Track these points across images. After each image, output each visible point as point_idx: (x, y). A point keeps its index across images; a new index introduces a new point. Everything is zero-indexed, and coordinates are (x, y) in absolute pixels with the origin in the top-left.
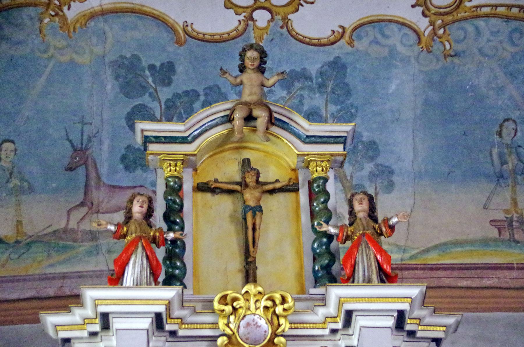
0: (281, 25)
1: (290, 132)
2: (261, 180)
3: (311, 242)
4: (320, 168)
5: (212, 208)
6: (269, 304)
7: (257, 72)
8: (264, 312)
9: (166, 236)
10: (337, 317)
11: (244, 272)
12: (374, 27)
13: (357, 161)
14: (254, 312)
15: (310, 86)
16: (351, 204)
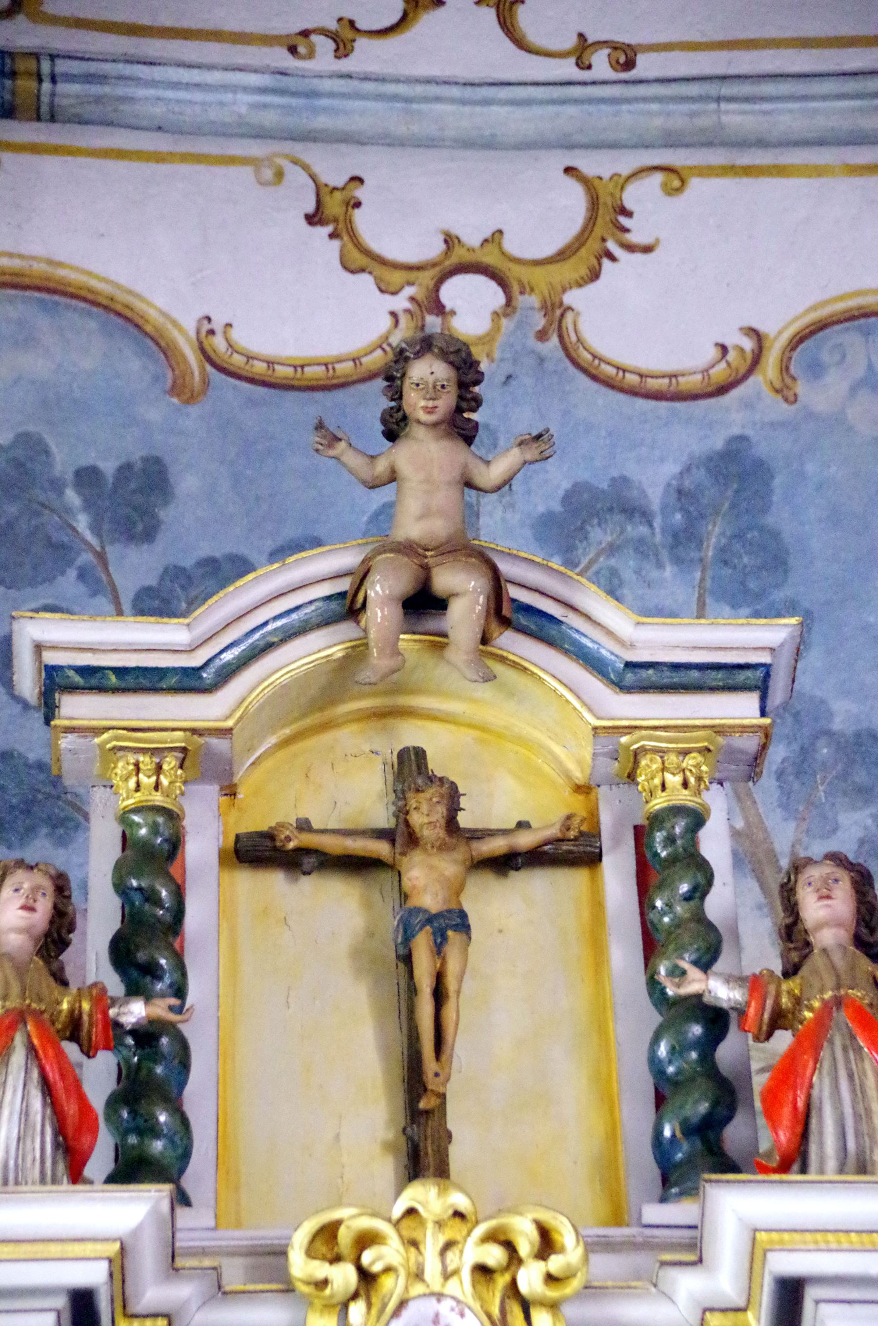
0: (540, 327)
1: (566, 652)
2: (464, 820)
3: (649, 1035)
4: (674, 774)
5: (290, 923)
6: (494, 1255)
7: (448, 435)
8: (474, 1287)
9: (118, 1014)
10: (744, 1310)
11: (405, 1154)
12: (867, 333)
13: (810, 803)
14: (436, 1287)
15: (641, 541)
16: (789, 901)
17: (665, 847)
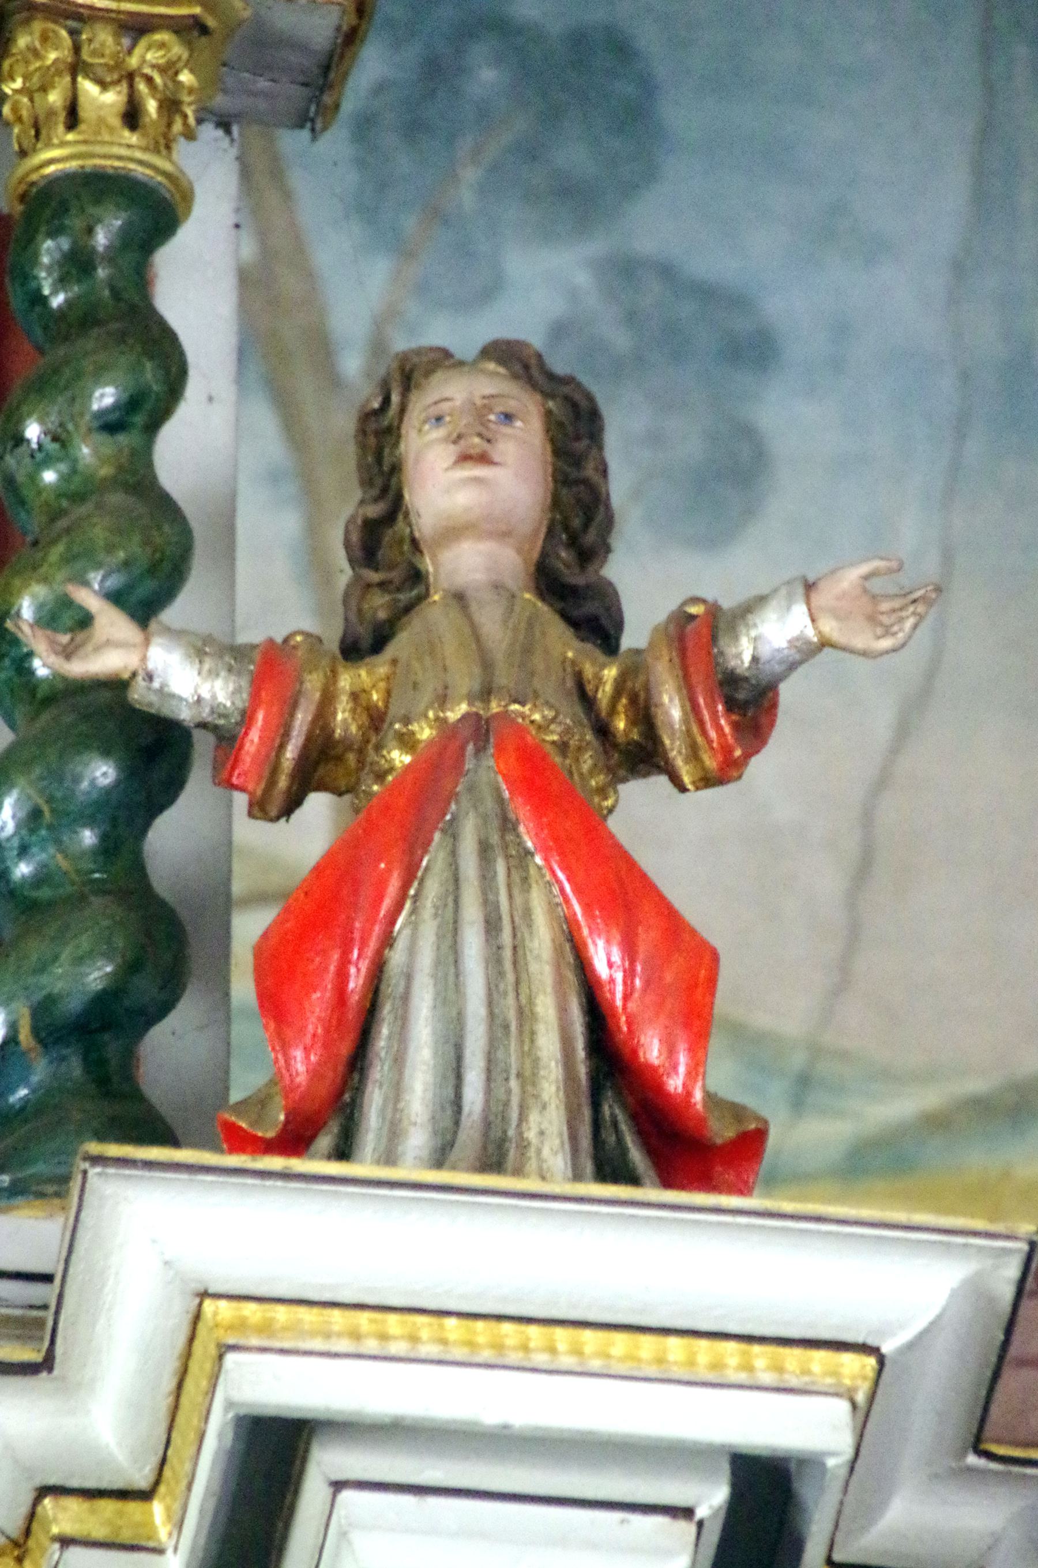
4: (104, 85)
10: (146, 1495)
17: (62, 282)
